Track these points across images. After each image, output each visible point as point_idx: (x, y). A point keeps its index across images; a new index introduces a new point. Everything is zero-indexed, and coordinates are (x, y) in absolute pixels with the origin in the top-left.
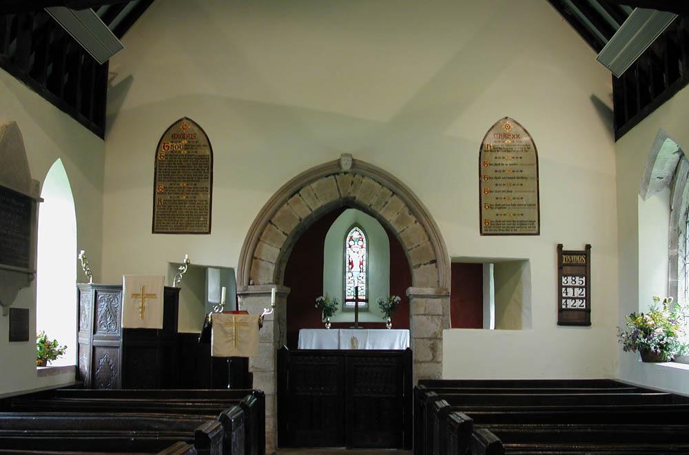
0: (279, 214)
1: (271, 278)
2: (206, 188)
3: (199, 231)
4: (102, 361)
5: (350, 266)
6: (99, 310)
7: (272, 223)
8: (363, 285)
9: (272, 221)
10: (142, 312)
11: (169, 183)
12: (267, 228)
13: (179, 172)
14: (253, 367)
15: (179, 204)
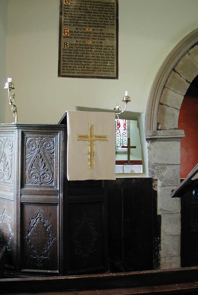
0: (181, 63)
1: (177, 123)
2: (112, 34)
3: (107, 76)
4: (33, 221)
5: (118, 126)
6: (28, 156)
7: (175, 71)
8: (126, 138)
9: (176, 69)
10: (91, 160)
11: (75, 27)
12: (171, 75)
13: (85, 18)
14: (161, 210)
15: (86, 48)
